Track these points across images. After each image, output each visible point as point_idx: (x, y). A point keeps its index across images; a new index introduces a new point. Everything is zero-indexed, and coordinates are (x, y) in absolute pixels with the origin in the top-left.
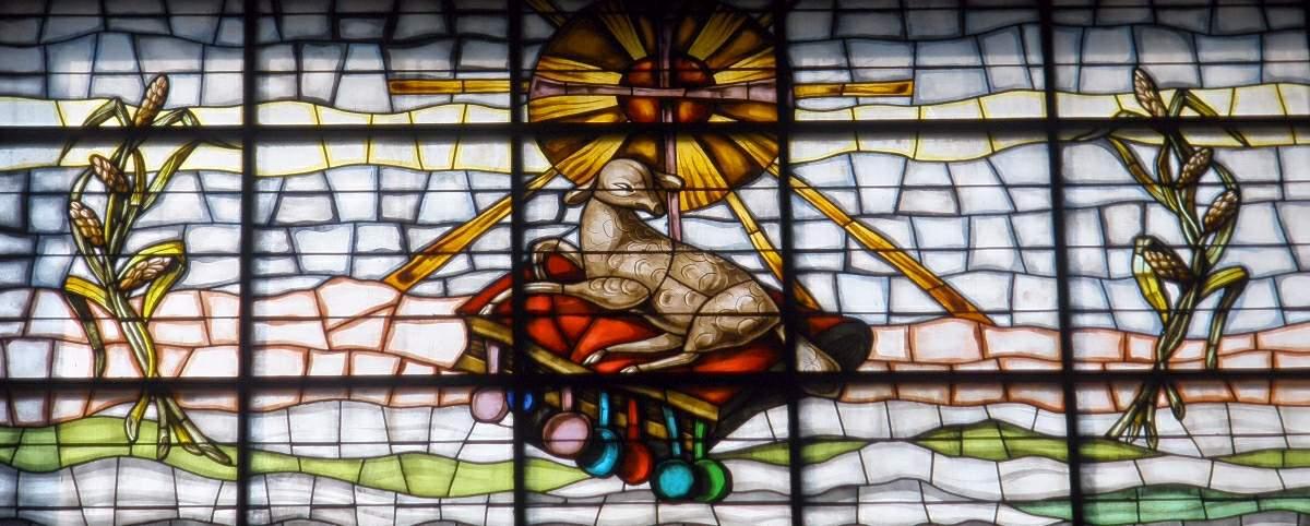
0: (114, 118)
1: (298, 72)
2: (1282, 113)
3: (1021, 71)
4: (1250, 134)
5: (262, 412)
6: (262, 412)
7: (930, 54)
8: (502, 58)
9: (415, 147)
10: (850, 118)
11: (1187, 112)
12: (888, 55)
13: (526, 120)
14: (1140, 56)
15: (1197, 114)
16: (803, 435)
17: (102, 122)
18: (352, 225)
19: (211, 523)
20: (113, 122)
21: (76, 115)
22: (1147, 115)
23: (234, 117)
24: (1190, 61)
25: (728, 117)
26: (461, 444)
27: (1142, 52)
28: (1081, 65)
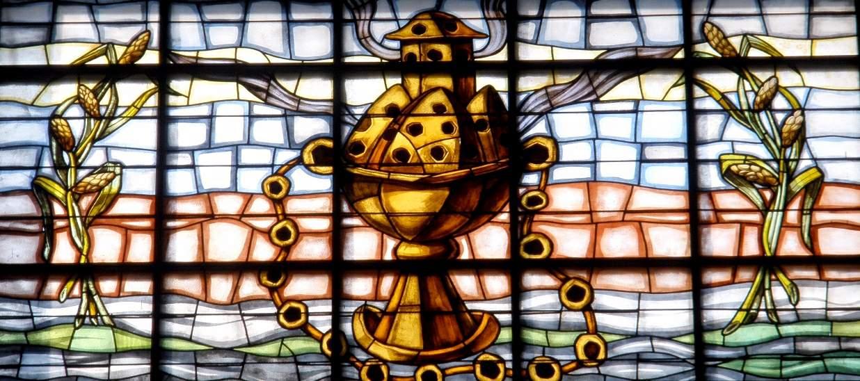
0: (104, 57)
1: (243, 23)
2: (44, 63)
3: (90, 27)
4: (280, 78)
5: (710, 286)
6: (710, 286)
7: (211, 13)
8: (239, 13)
9: (383, 80)
10: (43, 62)
11: (754, 53)
12: (831, 6)
13: (418, 60)
14: (763, 9)
15: (770, 56)
16: (454, 315)
17: (87, 61)
18: (105, 148)
19: (637, 379)
20: (102, 61)
21: (64, 55)
22: (720, 56)
23: (502, 56)
24: (89, 21)
25: (767, 53)
26: (736, 311)
27: (249, 13)
28: (372, 19)
